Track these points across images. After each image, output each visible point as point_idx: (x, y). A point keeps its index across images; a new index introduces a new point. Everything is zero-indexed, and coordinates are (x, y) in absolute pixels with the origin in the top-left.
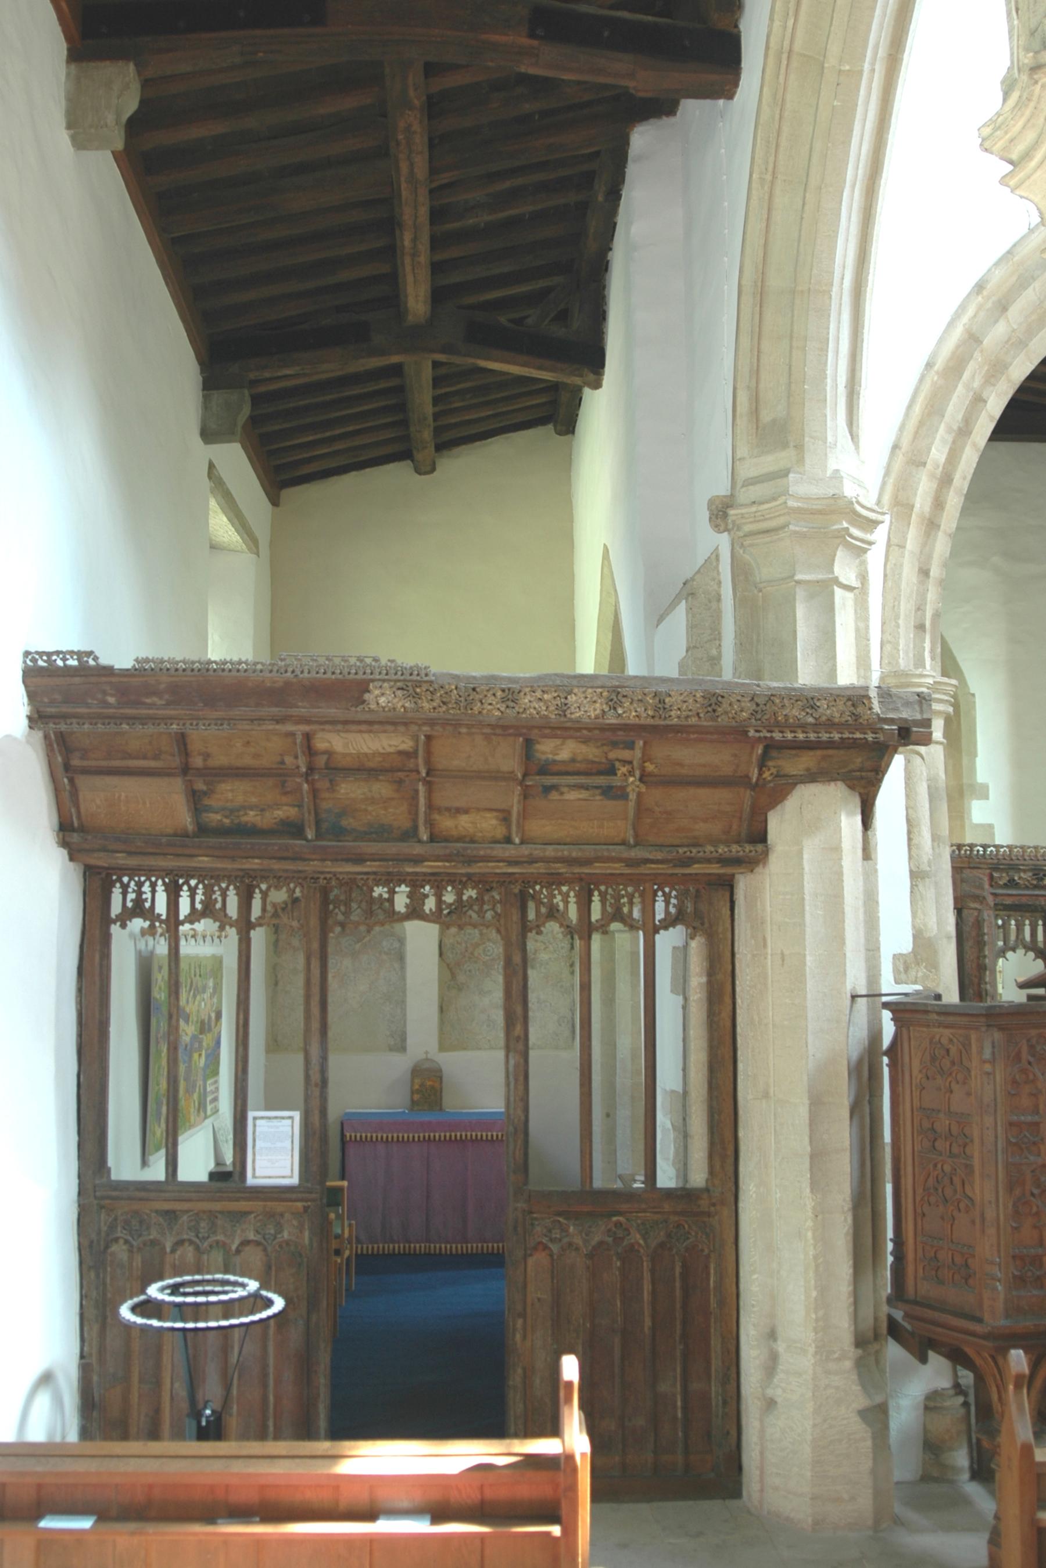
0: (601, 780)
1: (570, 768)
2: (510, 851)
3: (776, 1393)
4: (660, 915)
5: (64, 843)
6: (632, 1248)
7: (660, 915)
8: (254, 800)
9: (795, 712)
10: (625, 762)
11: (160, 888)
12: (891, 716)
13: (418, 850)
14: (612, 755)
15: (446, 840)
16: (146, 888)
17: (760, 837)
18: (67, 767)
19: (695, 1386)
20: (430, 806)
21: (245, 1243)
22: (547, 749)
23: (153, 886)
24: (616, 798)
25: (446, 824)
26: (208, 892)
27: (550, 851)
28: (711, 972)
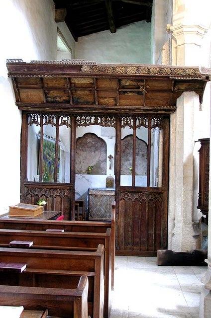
0: (136, 90)
1: (129, 87)
2: (116, 107)
3: (174, 232)
4: (152, 124)
5: (17, 105)
6: (144, 200)
7: (152, 124)
8: (58, 95)
9: (180, 72)
10: (142, 86)
11: (39, 117)
12: (204, 74)
13: (95, 107)
14: (138, 84)
15: (102, 105)
16: (36, 117)
17: (175, 104)
18: (17, 87)
19: (157, 232)
20: (98, 97)
21: (57, 195)
22: (124, 83)
23: (37, 116)
24: (141, 95)
25: (102, 101)
26: (50, 117)
27: (125, 107)
28: (164, 138)
